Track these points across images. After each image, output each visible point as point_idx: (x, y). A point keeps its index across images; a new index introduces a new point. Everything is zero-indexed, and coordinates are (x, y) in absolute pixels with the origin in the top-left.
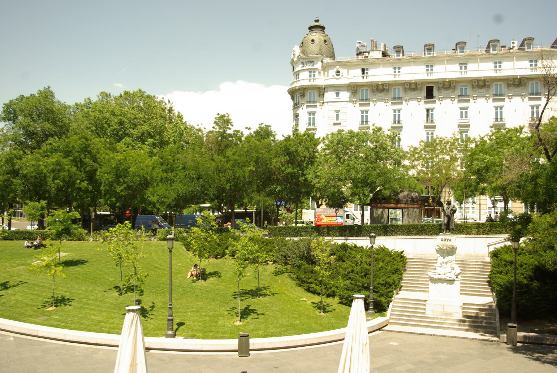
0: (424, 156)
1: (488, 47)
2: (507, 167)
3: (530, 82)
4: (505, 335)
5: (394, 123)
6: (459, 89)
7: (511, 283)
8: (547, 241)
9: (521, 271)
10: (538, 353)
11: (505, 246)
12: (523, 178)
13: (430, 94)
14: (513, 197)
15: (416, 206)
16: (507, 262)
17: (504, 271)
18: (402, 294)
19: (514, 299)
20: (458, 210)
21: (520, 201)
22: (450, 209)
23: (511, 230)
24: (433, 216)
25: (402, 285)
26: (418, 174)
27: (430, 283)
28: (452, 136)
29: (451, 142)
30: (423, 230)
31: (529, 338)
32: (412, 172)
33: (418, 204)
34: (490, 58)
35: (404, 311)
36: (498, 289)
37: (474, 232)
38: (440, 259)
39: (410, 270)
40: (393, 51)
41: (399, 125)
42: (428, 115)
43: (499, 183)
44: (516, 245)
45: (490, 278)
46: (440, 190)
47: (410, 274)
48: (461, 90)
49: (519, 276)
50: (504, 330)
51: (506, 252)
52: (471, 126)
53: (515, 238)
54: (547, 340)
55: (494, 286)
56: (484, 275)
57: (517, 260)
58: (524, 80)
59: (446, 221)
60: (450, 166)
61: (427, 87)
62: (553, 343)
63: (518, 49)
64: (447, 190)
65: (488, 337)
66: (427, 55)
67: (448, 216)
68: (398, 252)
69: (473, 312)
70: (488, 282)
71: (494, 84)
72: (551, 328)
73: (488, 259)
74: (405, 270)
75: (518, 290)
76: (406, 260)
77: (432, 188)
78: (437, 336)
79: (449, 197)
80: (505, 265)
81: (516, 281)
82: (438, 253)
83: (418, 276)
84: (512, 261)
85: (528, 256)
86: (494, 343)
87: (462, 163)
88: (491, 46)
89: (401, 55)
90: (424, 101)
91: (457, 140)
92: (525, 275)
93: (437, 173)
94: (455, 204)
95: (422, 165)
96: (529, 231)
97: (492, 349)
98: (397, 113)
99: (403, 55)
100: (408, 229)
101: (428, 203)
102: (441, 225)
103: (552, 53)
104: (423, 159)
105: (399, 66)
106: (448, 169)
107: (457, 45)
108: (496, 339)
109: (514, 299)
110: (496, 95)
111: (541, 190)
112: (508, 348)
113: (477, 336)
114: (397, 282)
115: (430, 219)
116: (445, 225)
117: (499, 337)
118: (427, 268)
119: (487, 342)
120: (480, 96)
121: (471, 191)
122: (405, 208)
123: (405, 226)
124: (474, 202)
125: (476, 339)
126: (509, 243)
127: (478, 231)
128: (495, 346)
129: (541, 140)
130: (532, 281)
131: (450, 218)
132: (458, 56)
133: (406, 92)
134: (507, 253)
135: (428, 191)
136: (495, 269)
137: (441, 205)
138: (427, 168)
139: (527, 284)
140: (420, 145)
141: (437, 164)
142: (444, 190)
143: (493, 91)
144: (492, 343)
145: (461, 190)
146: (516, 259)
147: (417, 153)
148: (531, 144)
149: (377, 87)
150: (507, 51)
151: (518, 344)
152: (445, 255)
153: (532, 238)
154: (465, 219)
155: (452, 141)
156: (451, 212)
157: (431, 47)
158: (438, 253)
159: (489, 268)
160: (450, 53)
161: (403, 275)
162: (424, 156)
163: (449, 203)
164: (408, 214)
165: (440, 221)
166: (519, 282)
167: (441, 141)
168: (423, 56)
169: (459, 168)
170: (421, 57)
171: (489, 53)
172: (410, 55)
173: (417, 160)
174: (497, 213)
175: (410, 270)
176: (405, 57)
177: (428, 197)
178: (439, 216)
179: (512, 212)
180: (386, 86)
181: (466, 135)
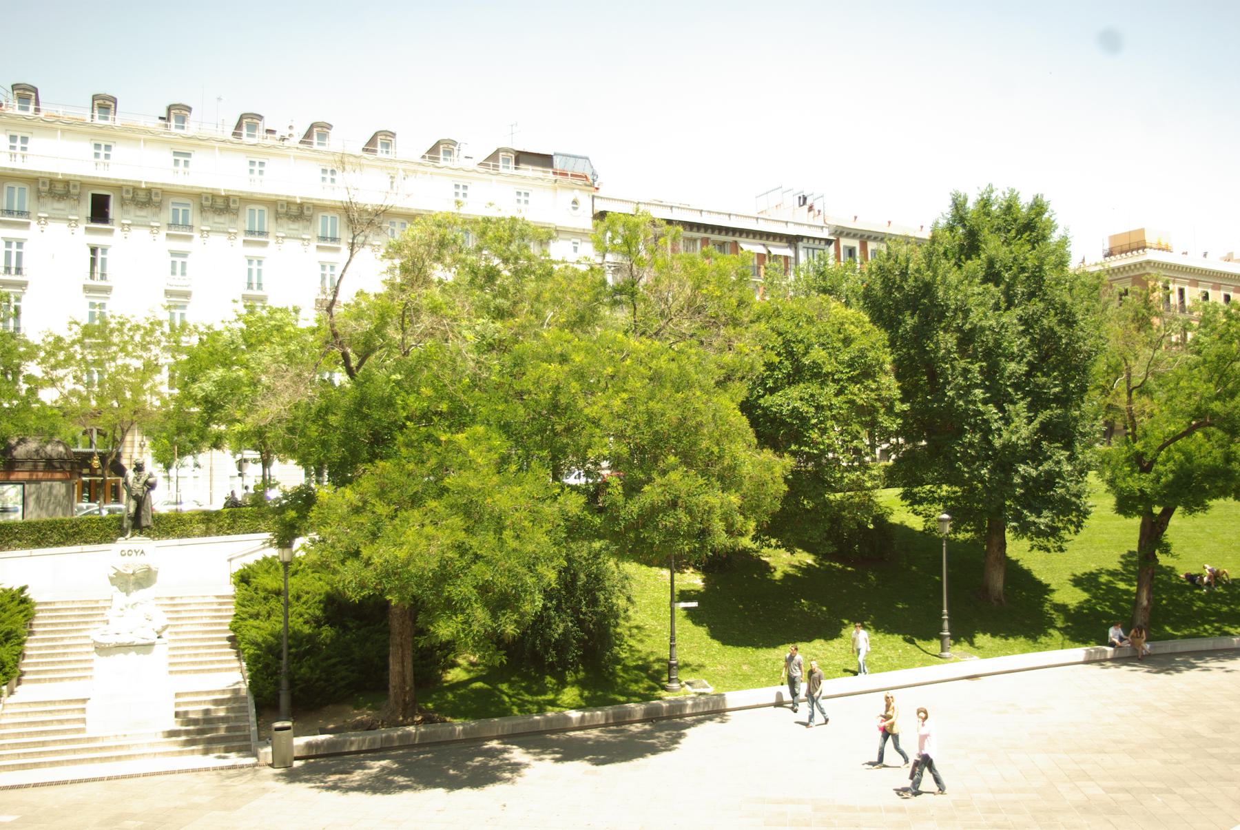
0: (79, 357)
1: (239, 126)
2: (268, 388)
3: (320, 215)
4: (269, 749)
5: (5, 272)
6: (171, 211)
7: (277, 636)
8: (346, 541)
9: (297, 608)
10: (335, 773)
11: (265, 559)
12: (300, 413)
13: (100, 211)
14: (280, 452)
15: (58, 476)
16: (269, 592)
17: (264, 613)
18: (24, 692)
19: (284, 669)
20: (161, 483)
21: (295, 461)
22: (141, 481)
23: (276, 523)
24: (102, 500)
25: (24, 669)
26: (66, 398)
27: (95, 656)
28: (149, 315)
29: (145, 328)
30: (76, 533)
31: (317, 746)
32: (48, 396)
33: (64, 471)
34: (241, 151)
35: (30, 734)
36: (252, 651)
37: (197, 531)
38: (119, 597)
39: (45, 632)
40: (10, 96)
41: (18, 278)
42: (93, 261)
43: (250, 423)
44: (285, 555)
45: (234, 630)
46: (118, 437)
47: (43, 640)
48: (175, 211)
49: (294, 618)
50: (264, 739)
51: (267, 571)
52: (193, 295)
53: (284, 541)
54: (352, 743)
55: (242, 646)
56: (220, 624)
57: (290, 587)
58: (308, 209)
59: (132, 510)
60: (143, 381)
61: (93, 195)
62: (364, 748)
63: (301, 142)
64: (138, 438)
65: (234, 758)
66: (97, 121)
67: (137, 499)
68: (11, 589)
69: (195, 711)
70: (230, 639)
71: (247, 211)
72: (359, 718)
73: (230, 590)
74: (31, 633)
75: (293, 650)
76: (32, 607)
77: (99, 432)
78: (117, 778)
79: (141, 453)
80: (265, 598)
81: (288, 631)
82: (113, 585)
83: (66, 642)
84: (280, 590)
85: (311, 575)
86: (246, 770)
87: (172, 377)
88: (244, 125)
89: (32, 107)
90: (86, 228)
91: (160, 324)
92: (306, 616)
93: (112, 399)
94: (153, 468)
95: (75, 377)
96: (312, 524)
97: (242, 785)
98: (14, 249)
99: (37, 110)
100: (39, 532)
101: (90, 466)
102: (121, 519)
103: (363, 161)
104: (79, 365)
105: (108, 144)
106: (137, 390)
107: (169, 109)
108: (252, 760)
109: (284, 669)
110: (251, 232)
111: (335, 438)
112: (276, 775)
113: (211, 760)
114: (11, 664)
115: (95, 506)
116: (129, 518)
117: (256, 755)
118: (86, 623)
119: (231, 772)
120: (54, 218)
121: (191, 441)
122: (30, 481)
123: (29, 525)
124: (197, 465)
125: (207, 769)
126: (273, 552)
127: (208, 529)
128: (249, 776)
129: (335, 335)
130: (319, 626)
131: (140, 502)
132: (170, 134)
133: (41, 200)
134: (269, 573)
135: (91, 442)
136: (244, 609)
137: (120, 470)
138: (90, 384)
139: (310, 636)
140: (70, 330)
141: (112, 378)
142: (128, 438)
143: (244, 223)
144: (242, 770)
145: (169, 438)
146: (286, 585)
147: (62, 349)
148: (318, 343)
149: (51, 185)
150: (277, 143)
151: (297, 764)
152: (131, 587)
153: (317, 538)
154: (177, 503)
155: (148, 326)
156: (145, 489)
157: (108, 103)
158: (113, 584)
159: (231, 610)
160: (156, 124)
161: (27, 645)
162: (79, 357)
163: (139, 468)
164: (38, 499)
165: (120, 510)
166: (294, 632)
167: (122, 324)
168: (88, 120)
169: (165, 389)
170: (84, 123)
171: (240, 141)
172: (56, 114)
173: (63, 367)
174: (246, 488)
175: (45, 632)
176: (42, 115)
177: (91, 455)
178: (117, 499)
179: (277, 484)
180: (157, 194)
181: (182, 315)
